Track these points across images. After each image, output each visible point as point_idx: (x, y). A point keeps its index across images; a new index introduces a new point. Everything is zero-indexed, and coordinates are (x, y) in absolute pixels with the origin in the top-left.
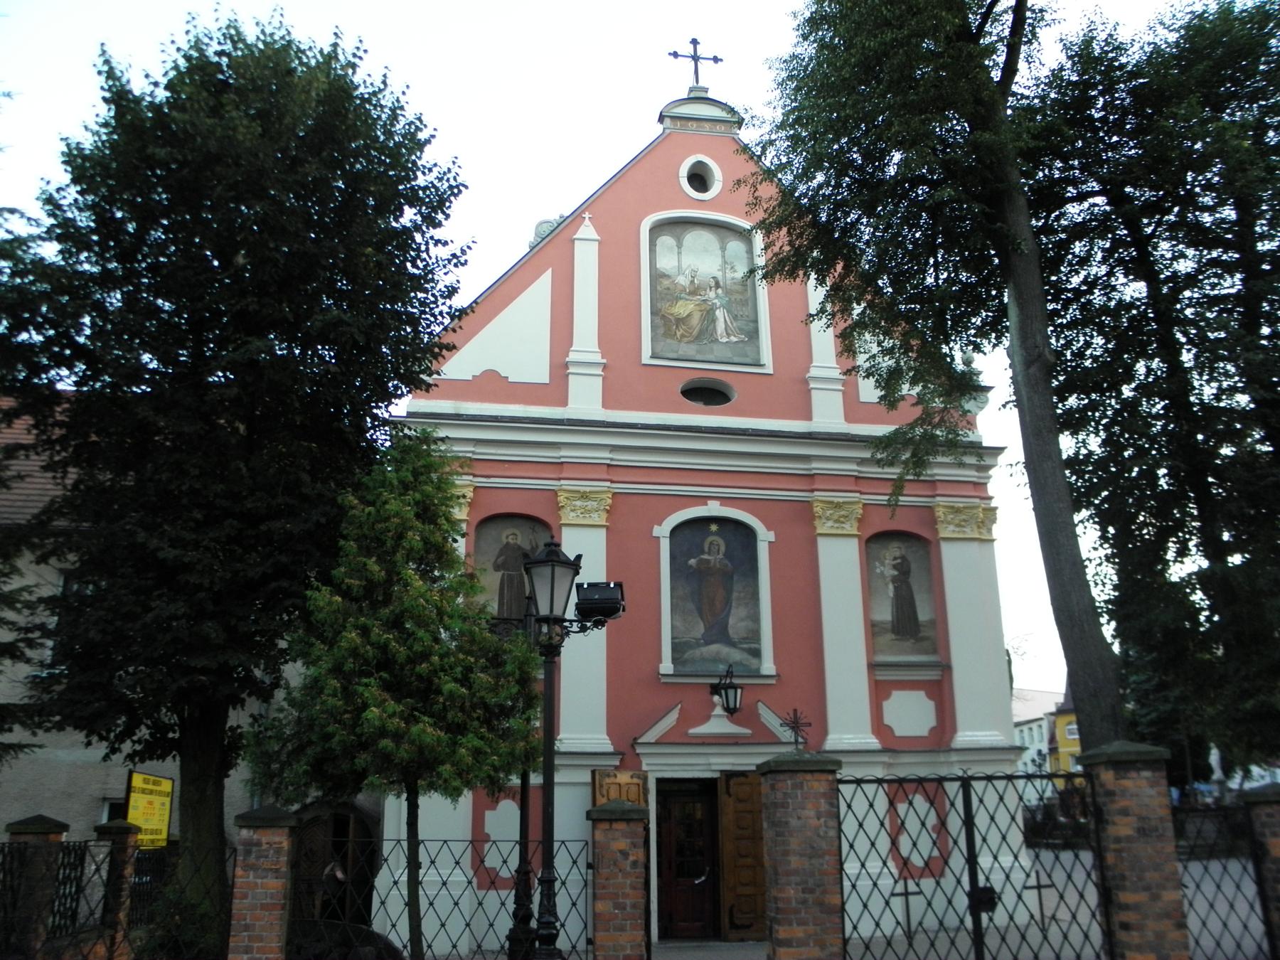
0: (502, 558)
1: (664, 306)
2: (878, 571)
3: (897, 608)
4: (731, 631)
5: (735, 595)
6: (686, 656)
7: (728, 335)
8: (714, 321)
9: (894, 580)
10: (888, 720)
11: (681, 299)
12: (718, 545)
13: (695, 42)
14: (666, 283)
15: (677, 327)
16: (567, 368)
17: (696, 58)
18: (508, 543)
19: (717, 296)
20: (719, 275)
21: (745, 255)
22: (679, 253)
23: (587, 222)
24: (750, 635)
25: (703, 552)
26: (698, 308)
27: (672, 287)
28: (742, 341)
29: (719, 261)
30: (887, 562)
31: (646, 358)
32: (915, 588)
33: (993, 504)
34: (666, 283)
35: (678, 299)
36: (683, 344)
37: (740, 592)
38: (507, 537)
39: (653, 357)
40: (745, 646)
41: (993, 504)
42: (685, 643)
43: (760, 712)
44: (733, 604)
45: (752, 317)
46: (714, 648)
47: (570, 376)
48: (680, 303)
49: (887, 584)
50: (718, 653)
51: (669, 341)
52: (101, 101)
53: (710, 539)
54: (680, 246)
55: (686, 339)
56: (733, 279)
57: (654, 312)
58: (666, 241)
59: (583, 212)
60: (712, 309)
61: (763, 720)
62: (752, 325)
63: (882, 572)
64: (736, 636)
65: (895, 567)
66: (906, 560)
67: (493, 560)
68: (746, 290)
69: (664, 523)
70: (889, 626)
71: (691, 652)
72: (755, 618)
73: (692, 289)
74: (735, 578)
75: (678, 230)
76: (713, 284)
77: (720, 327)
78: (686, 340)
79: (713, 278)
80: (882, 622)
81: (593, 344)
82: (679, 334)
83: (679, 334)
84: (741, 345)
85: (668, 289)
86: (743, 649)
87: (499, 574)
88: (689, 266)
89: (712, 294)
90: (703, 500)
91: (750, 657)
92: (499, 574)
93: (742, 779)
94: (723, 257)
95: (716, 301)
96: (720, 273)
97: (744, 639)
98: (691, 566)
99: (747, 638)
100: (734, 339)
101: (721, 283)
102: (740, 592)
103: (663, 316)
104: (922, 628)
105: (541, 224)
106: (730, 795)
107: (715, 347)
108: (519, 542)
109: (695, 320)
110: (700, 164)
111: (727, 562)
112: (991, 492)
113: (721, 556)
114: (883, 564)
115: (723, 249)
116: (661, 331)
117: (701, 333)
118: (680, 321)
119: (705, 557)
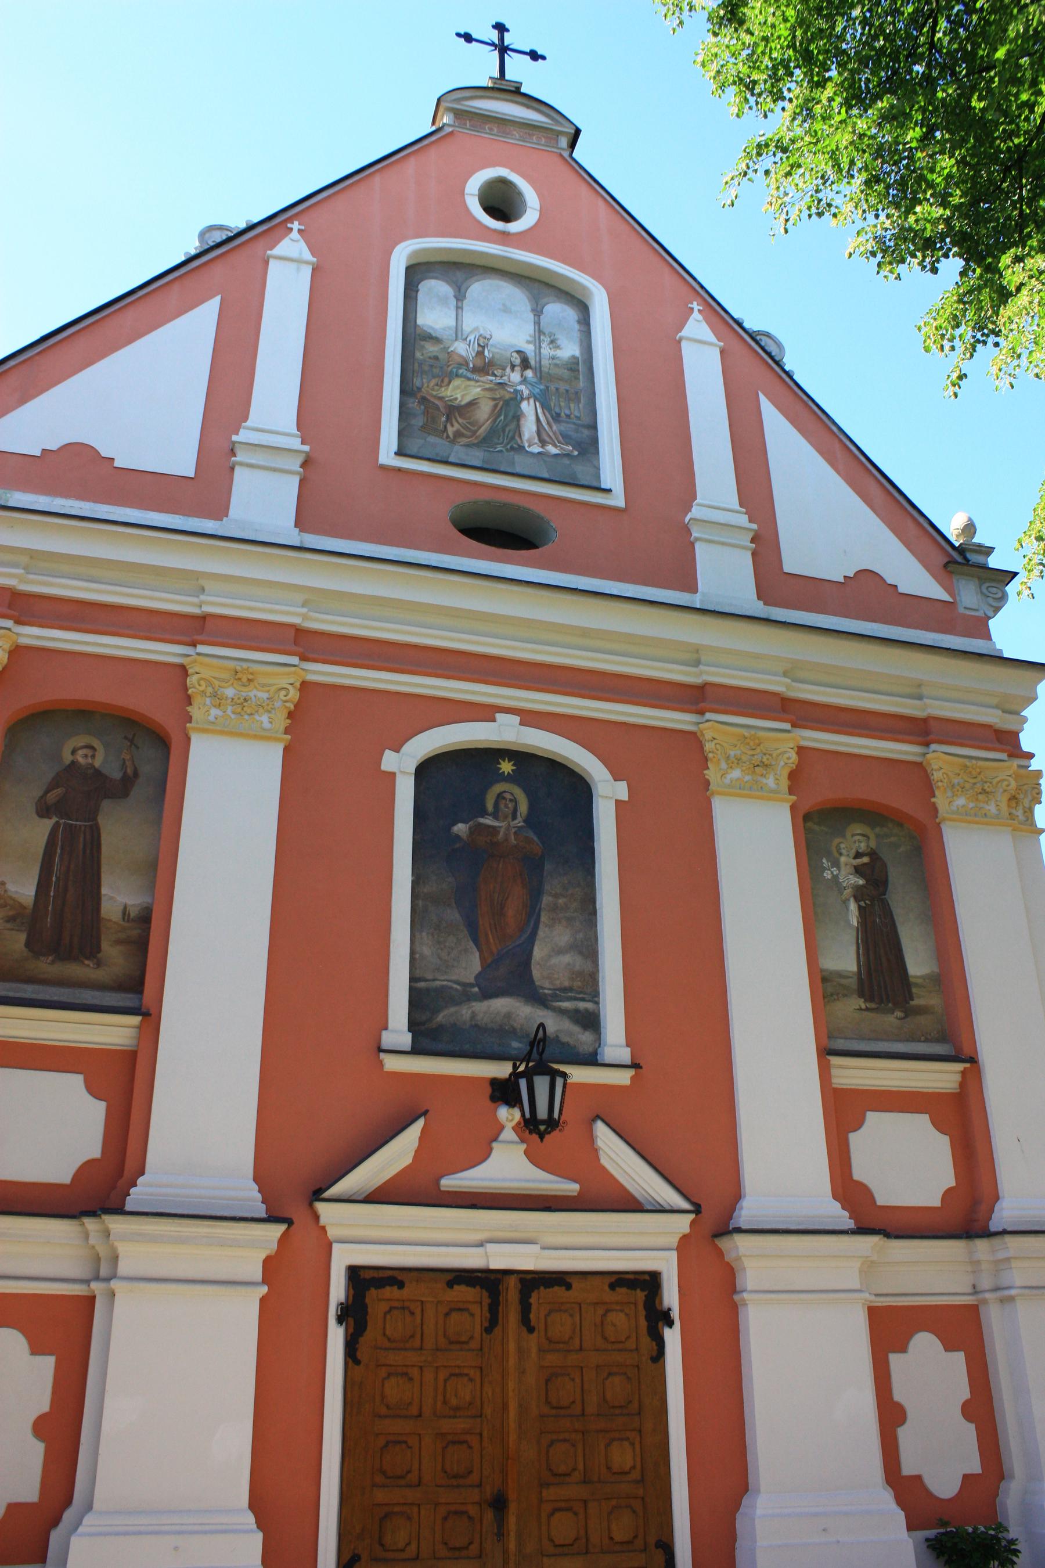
0: (59, 791)
1: (427, 385)
2: (827, 875)
3: (866, 943)
4: (536, 973)
5: (546, 900)
6: (441, 1018)
7: (543, 443)
8: (518, 417)
9: (858, 894)
10: (860, 1172)
11: (457, 376)
12: (515, 801)
13: (501, 28)
14: (431, 349)
15: (448, 419)
16: (233, 453)
17: (503, 50)
18: (73, 763)
19: (524, 381)
20: (529, 349)
21: (577, 326)
22: (459, 308)
23: (294, 234)
24: (577, 984)
25: (484, 813)
26: (488, 394)
27: (442, 356)
28: (568, 455)
29: (530, 328)
30: (843, 859)
31: (387, 453)
32: (899, 914)
33: (1035, 765)
34: (431, 349)
35: (452, 376)
36: (457, 448)
37: (556, 896)
38: (74, 752)
39: (399, 453)
40: (566, 1005)
41: (1035, 765)
42: (440, 991)
43: (600, 1143)
44: (544, 918)
45: (586, 420)
46: (501, 1005)
47: (238, 470)
48: (456, 382)
49: (845, 902)
50: (508, 1016)
51: (432, 439)
52: (1022, 1551)
53: (498, 788)
54: (460, 297)
55: (464, 441)
56: (553, 358)
57: (406, 390)
58: (434, 288)
59: (290, 220)
60: (514, 399)
61: (604, 1161)
62: (586, 432)
63: (835, 878)
64: (547, 984)
65: (858, 870)
66: (879, 858)
67: (37, 793)
68: (577, 378)
69: (406, 748)
70: (853, 983)
71: (452, 1010)
72: (590, 950)
73: (479, 363)
74: (548, 867)
75: (460, 275)
76: (517, 361)
77: (529, 428)
78: (464, 441)
79: (519, 352)
80: (840, 975)
81: (288, 420)
82: (451, 430)
83: (451, 430)
84: (566, 461)
85: (436, 358)
86: (562, 1012)
87: (48, 824)
88: (476, 329)
89: (515, 377)
90: (487, 713)
91: (576, 1029)
92: (48, 824)
93: (558, 1291)
94: (537, 323)
95: (522, 387)
96: (531, 347)
97: (565, 990)
98: (457, 836)
99: (570, 989)
100: (552, 450)
101: (532, 362)
102: (556, 896)
103: (424, 400)
104: (914, 990)
105: (211, 228)
106: (531, 1330)
107: (518, 458)
108: (97, 763)
109: (484, 410)
110: (503, 182)
111: (531, 834)
112: (1027, 743)
113: (519, 822)
114: (836, 864)
115: (538, 312)
116: (419, 421)
117: (493, 432)
118: (454, 410)
119: (488, 821)
